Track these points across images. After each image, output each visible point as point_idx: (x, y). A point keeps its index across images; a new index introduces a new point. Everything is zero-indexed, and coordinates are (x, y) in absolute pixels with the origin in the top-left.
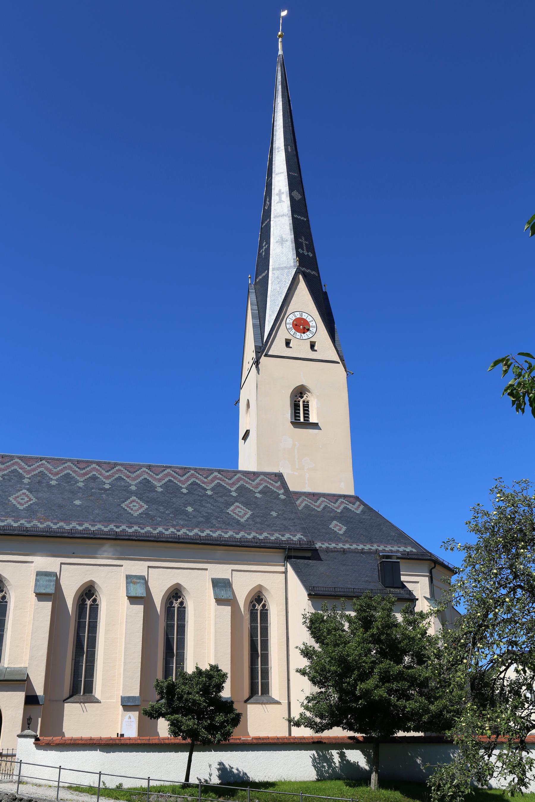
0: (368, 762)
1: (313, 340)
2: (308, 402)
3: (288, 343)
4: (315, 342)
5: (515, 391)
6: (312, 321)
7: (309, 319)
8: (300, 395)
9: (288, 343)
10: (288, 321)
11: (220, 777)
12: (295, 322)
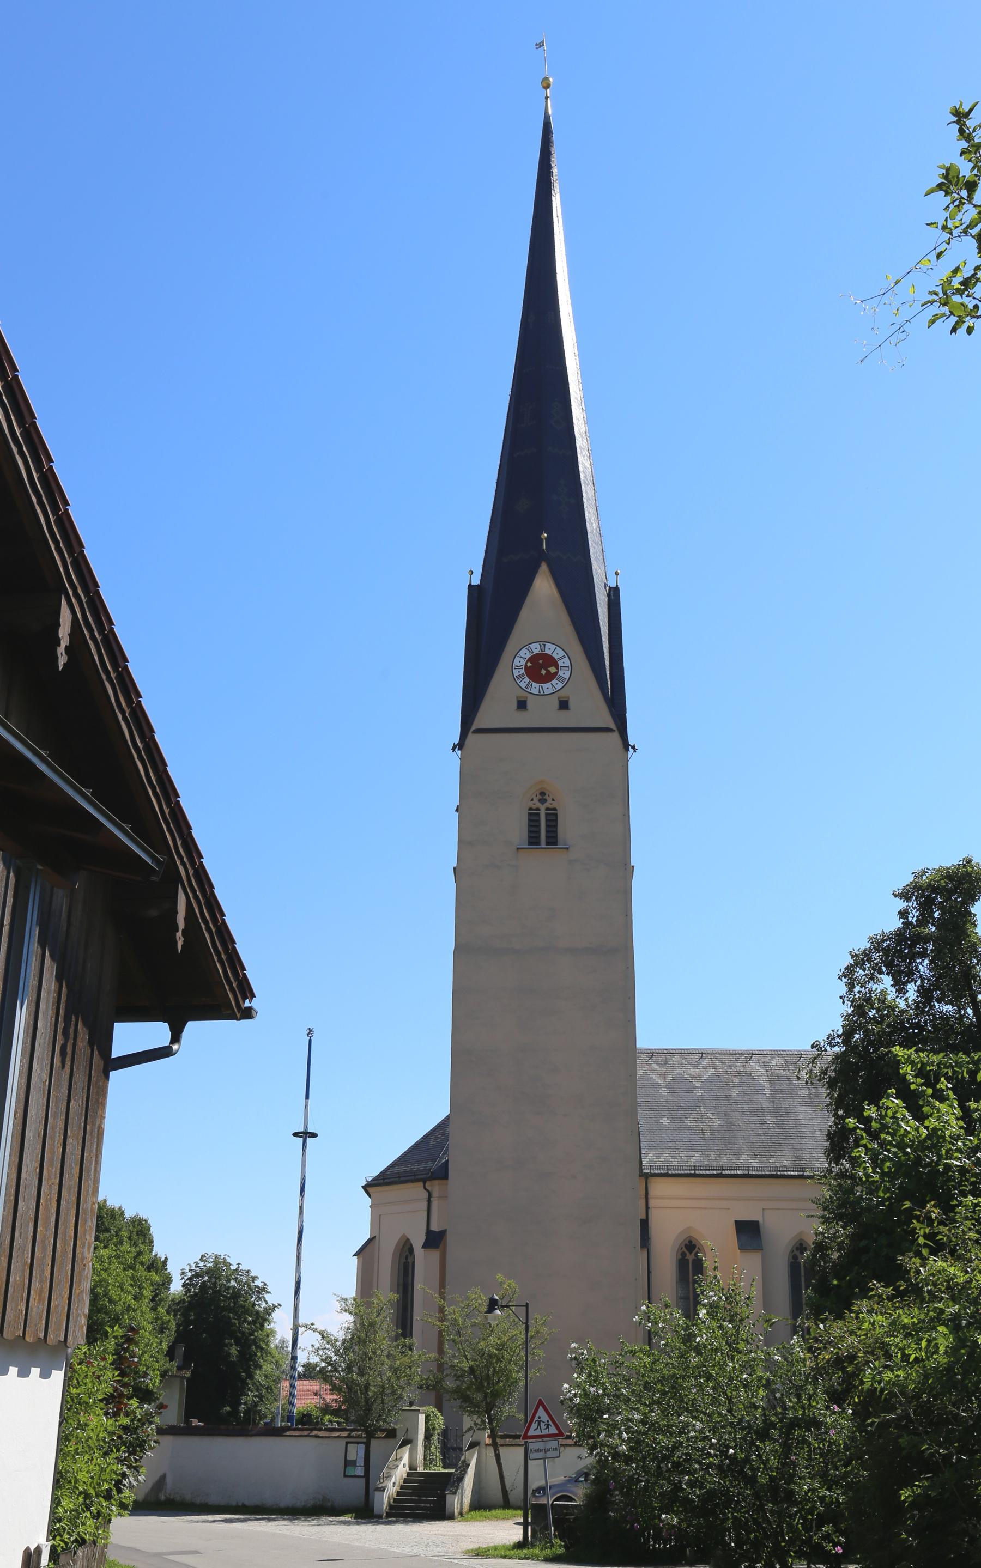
5: (841, 1112)
6: (564, 657)
7: (558, 654)
8: (539, 797)
12: (529, 664)
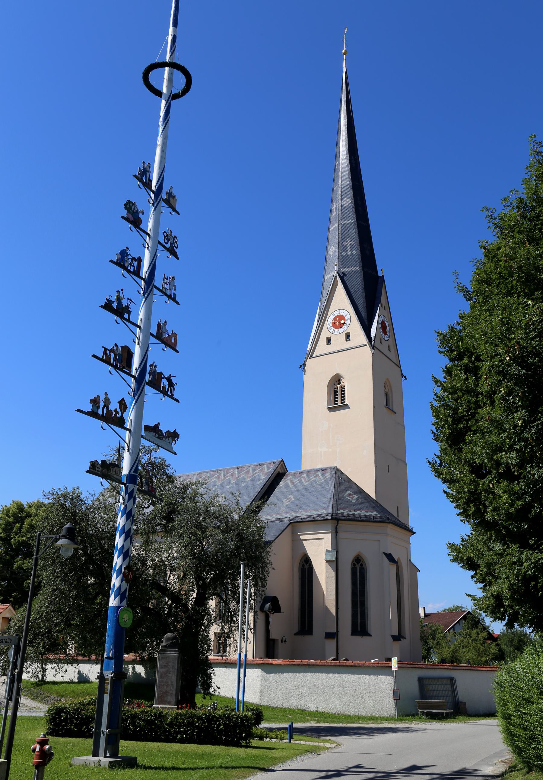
0: (146, 673)
1: (347, 332)
3: (329, 341)
9: (329, 341)
11: (78, 678)
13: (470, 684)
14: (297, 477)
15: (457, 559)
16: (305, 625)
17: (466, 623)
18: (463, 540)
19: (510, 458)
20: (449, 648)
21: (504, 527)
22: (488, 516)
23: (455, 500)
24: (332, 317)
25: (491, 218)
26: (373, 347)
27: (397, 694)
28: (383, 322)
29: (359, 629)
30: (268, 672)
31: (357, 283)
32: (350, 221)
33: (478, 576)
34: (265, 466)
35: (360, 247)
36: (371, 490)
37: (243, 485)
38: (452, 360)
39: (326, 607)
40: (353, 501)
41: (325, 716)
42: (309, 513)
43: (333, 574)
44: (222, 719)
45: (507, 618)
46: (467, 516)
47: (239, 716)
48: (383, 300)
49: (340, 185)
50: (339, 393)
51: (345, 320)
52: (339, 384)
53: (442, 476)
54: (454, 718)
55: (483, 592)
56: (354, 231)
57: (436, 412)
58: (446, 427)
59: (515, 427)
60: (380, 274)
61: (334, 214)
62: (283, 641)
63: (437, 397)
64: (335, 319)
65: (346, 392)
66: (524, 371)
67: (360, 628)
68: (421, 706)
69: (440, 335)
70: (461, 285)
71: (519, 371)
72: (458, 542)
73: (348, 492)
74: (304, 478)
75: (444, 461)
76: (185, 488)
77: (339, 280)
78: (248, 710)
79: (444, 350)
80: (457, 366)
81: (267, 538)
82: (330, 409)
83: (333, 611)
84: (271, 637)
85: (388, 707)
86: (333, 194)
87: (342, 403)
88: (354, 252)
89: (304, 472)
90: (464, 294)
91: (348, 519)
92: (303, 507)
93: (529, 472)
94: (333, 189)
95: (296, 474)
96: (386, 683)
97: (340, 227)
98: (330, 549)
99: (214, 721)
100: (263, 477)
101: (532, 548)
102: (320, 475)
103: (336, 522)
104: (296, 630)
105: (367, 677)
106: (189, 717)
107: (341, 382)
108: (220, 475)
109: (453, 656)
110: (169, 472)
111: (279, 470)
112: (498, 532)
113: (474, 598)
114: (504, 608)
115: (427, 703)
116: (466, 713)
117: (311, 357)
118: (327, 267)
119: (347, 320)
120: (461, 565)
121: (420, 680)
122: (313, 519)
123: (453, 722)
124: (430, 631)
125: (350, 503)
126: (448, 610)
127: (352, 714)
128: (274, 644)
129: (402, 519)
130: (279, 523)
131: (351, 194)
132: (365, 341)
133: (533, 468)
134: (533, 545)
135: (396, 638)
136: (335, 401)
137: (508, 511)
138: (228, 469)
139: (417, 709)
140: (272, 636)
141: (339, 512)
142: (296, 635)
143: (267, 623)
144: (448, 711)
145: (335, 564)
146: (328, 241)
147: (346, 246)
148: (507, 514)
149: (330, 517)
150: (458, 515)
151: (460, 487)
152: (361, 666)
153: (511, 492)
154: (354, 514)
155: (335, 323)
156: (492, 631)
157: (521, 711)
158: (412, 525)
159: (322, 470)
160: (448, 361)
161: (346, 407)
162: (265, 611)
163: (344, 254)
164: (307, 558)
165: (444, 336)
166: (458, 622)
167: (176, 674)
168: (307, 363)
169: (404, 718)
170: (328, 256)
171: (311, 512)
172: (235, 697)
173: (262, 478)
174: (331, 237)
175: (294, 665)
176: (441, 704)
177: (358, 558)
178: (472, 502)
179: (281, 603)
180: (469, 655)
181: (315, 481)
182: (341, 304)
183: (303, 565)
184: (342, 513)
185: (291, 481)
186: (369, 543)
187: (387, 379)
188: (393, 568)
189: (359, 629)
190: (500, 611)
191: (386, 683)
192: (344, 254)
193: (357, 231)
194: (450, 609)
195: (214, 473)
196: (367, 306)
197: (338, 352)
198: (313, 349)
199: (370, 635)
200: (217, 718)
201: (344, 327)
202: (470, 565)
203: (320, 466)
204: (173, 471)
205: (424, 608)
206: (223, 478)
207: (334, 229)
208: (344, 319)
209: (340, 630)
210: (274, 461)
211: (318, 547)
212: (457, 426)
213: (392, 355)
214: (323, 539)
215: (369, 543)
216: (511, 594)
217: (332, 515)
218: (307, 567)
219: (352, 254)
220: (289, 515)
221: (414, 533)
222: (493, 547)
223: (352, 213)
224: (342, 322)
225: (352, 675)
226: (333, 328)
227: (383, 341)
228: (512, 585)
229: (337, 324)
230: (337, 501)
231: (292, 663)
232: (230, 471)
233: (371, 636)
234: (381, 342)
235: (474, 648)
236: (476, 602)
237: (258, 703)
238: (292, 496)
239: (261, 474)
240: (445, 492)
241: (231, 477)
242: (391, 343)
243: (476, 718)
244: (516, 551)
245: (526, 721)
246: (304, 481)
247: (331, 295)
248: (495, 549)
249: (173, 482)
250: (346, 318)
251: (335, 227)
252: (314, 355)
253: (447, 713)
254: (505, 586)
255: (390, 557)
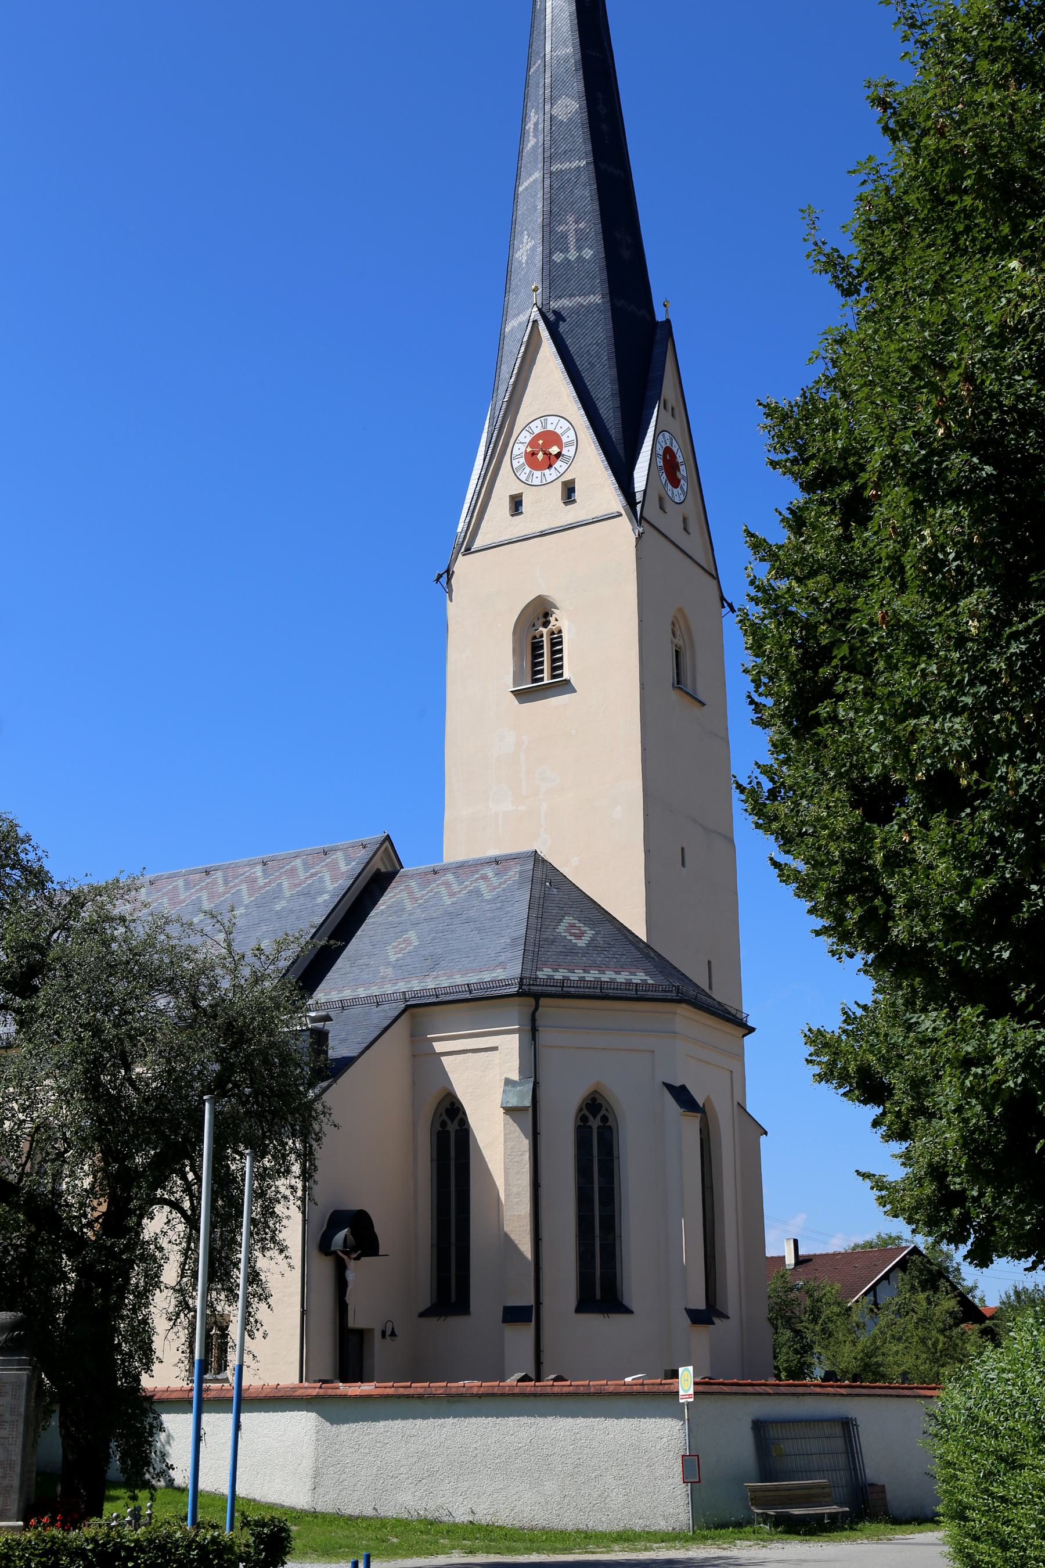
1: (567, 477)
2: (560, 631)
3: (516, 504)
4: (573, 481)
9: (516, 504)
10: (516, 452)
13: (894, 1435)
14: (429, 882)
15: (832, 1072)
16: (450, 1288)
17: (907, 1277)
18: (848, 1018)
19: (942, 732)
20: (854, 1343)
21: (941, 957)
22: (898, 931)
23: (806, 888)
24: (526, 437)
25: (912, 26)
26: (639, 520)
27: (693, 1467)
28: (668, 451)
29: (598, 1296)
30: (334, 1419)
31: (596, 341)
32: (574, 165)
33: (889, 1117)
34: (340, 854)
35: (605, 239)
36: (632, 914)
37: (278, 907)
38: (808, 487)
39: (506, 1236)
40: (581, 943)
41: (494, 1535)
42: (459, 980)
43: (525, 1144)
44: (144, 1552)
45: (972, 1236)
46: (844, 937)
47: (194, 1541)
48: (668, 389)
49: (548, 57)
50: (546, 650)
51: (560, 447)
52: (546, 624)
53: (775, 826)
54: (852, 1529)
55: (904, 1164)
56: (587, 193)
57: (754, 634)
58: (783, 675)
59: (961, 640)
60: (660, 317)
61: (531, 142)
62: (388, 1333)
63: (758, 588)
64: (533, 443)
65: (565, 646)
66: (988, 469)
67: (601, 1291)
68: (759, 1499)
69: (771, 411)
70: (827, 249)
71: (974, 469)
72: (833, 1024)
73: (568, 920)
74: (447, 884)
75: (783, 784)
76: (77, 901)
77: (544, 333)
78: (246, 1524)
79: (784, 457)
80: (822, 503)
81: (336, 1050)
82: (522, 696)
83: (526, 1247)
84: (351, 1324)
85: (669, 1503)
86: (527, 85)
87: (553, 677)
88: (588, 253)
89: (446, 869)
90: (835, 277)
91: (565, 993)
92: (443, 964)
93: (1003, 779)
94: (528, 69)
95: (426, 873)
96: (663, 1437)
97: (547, 182)
98: (515, 1076)
99: (120, 1559)
100: (332, 882)
101: (1021, 1014)
102: (490, 874)
103: (531, 1002)
104: (425, 1303)
105: (610, 1422)
106: (46, 1553)
107: (552, 619)
108: (214, 883)
109: (866, 1364)
110: (29, 857)
111: (378, 865)
112: (930, 977)
113: (879, 1184)
114: (963, 1207)
115: (777, 1489)
116: (886, 1513)
117: (468, 549)
118: (512, 297)
119: (569, 444)
120: (842, 1091)
121: (759, 1426)
122: (468, 996)
123: (848, 1538)
124: (808, 1302)
125: (572, 951)
126: (864, 1246)
127: (570, 1527)
128: (361, 1342)
129: (719, 995)
130: (375, 1009)
131: (576, 84)
132: (615, 501)
133: (1014, 764)
134: (1025, 1004)
135: (698, 1318)
136: (536, 672)
137: (953, 909)
138: (237, 866)
139: (750, 1509)
140: (354, 1322)
141: (540, 974)
142: (415, 1315)
143: (341, 1285)
144: (834, 1509)
145: (530, 1116)
146: (513, 222)
147: (564, 236)
148: (950, 916)
149: (514, 989)
150: (818, 933)
151: (819, 849)
152: (595, 1394)
153: (958, 853)
154: (582, 979)
155: (533, 454)
156: (982, 1300)
157: (992, 1495)
158: (751, 1009)
159: (496, 861)
160: (797, 487)
161: (566, 687)
162: (335, 1252)
163: (558, 257)
164: (453, 1104)
165: (785, 417)
166: (886, 1276)
167: (21, 1429)
168: (457, 568)
169: (713, 1532)
170: (515, 264)
171: (463, 975)
172: (226, 1490)
173: (330, 886)
174: (522, 209)
175: (408, 1396)
176: (813, 1491)
177: (594, 1100)
178: (850, 890)
179: (378, 1229)
180: (908, 1362)
181: (477, 893)
182: (551, 398)
183: (443, 1124)
184: (550, 978)
185: (411, 893)
186: (627, 1060)
187: (680, 610)
188: (692, 1124)
189: (598, 1296)
190: (951, 1215)
191: (663, 1437)
192: (558, 257)
193: (595, 192)
194: (869, 1245)
195: (197, 876)
196: (622, 407)
197: (543, 534)
198: (474, 530)
199: (629, 1311)
200: (128, 1549)
201: (559, 465)
202: (869, 1088)
203: (493, 852)
204: (40, 853)
205: (796, 1242)
206: (221, 890)
207: (531, 186)
208: (560, 444)
209: (545, 1299)
210: (365, 839)
211: (484, 1073)
212: (816, 673)
213: (694, 544)
214: (495, 1049)
215: (627, 1060)
216: (970, 1158)
217: (521, 984)
218: (452, 1127)
219: (580, 258)
220: (402, 987)
221: (752, 1030)
222: (917, 1023)
223: (580, 139)
224: (554, 450)
225: (570, 1420)
226: (528, 469)
227: (668, 505)
228: (973, 1133)
229: (540, 456)
230: (537, 944)
231: (402, 1391)
232: (241, 871)
233: (631, 1312)
234: (662, 508)
235: (923, 1341)
236: (884, 1193)
237: (306, 1507)
238: (412, 935)
239: (327, 878)
240: (776, 864)
241: (244, 887)
242: (691, 509)
243: (911, 1527)
244: (973, 1026)
245: (1007, 1522)
246: (447, 894)
247: (523, 376)
248: (923, 1027)
249: (42, 884)
250: (564, 439)
251: (532, 180)
252: (477, 545)
253: (833, 1516)
254: (952, 1135)
255: (682, 1096)
